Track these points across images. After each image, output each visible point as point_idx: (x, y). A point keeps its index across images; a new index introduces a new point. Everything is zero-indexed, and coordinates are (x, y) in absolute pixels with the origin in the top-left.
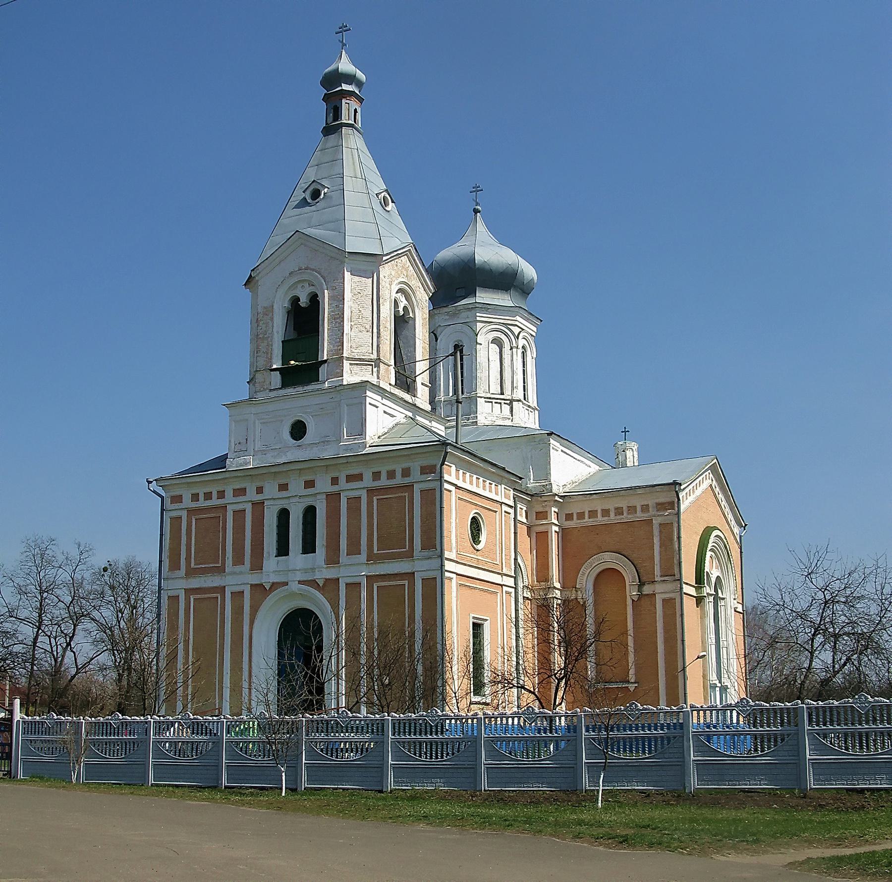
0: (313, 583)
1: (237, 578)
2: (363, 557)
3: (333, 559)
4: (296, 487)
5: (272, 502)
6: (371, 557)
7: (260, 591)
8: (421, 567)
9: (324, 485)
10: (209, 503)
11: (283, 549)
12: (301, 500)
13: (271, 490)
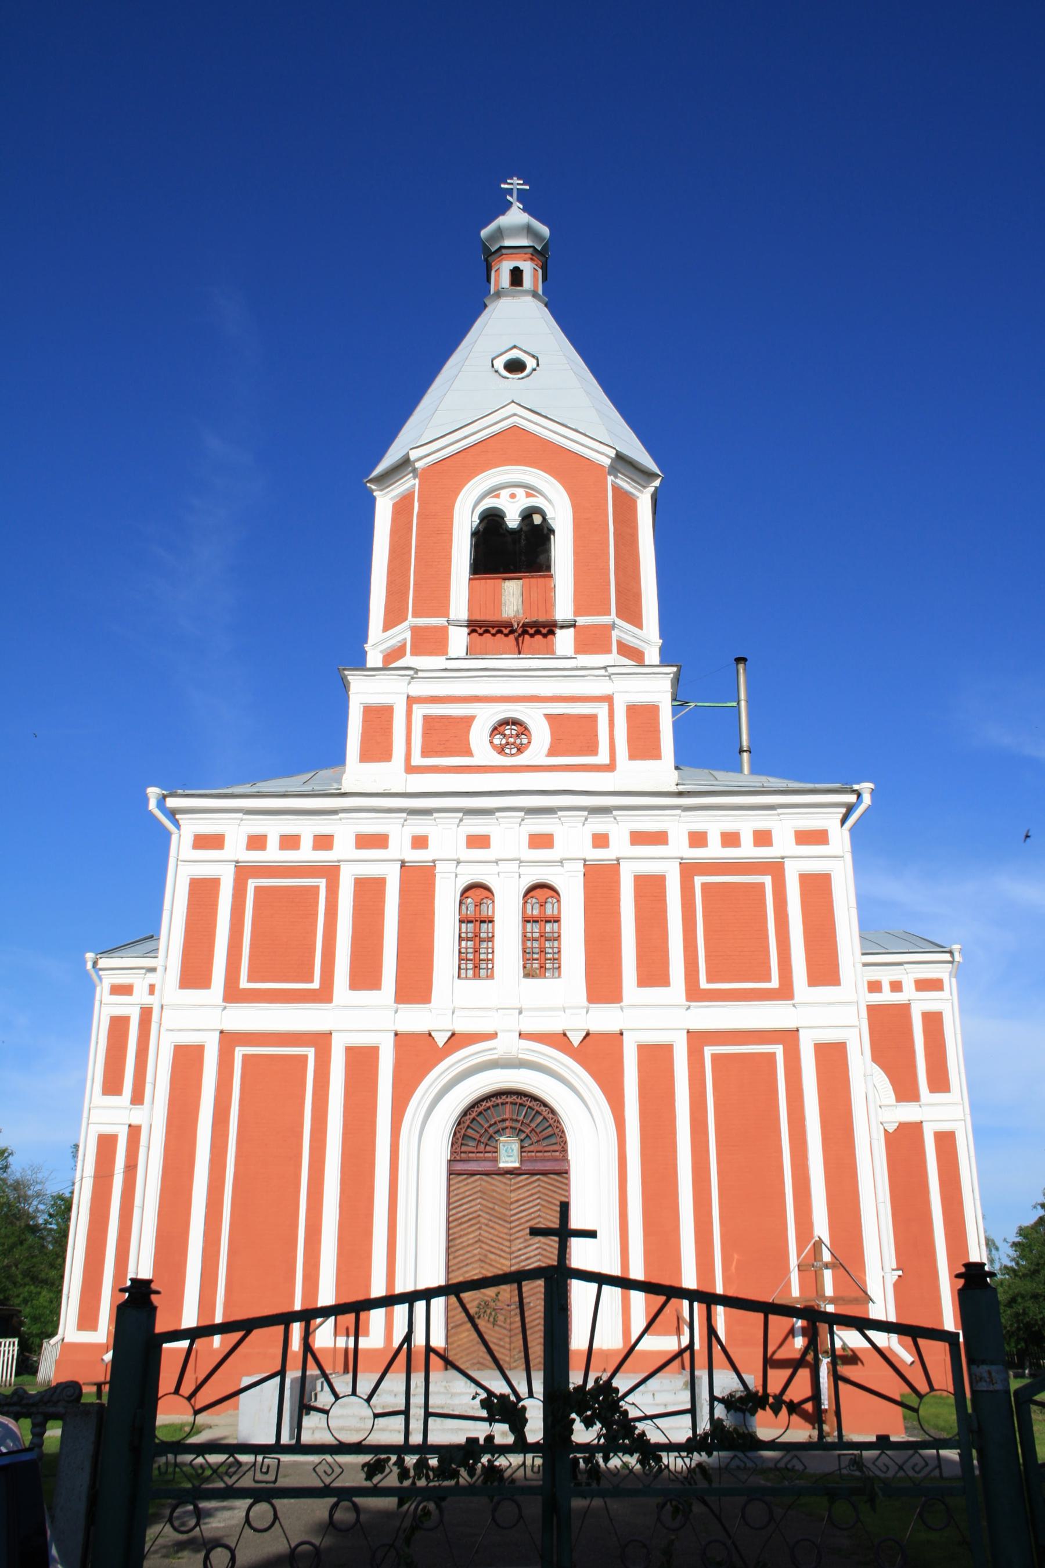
0: (559, 1040)
1: (363, 1018)
3: (603, 986)
4: (509, 835)
6: (694, 993)
7: (417, 1054)
10: (290, 856)
11: (476, 961)
12: (523, 870)
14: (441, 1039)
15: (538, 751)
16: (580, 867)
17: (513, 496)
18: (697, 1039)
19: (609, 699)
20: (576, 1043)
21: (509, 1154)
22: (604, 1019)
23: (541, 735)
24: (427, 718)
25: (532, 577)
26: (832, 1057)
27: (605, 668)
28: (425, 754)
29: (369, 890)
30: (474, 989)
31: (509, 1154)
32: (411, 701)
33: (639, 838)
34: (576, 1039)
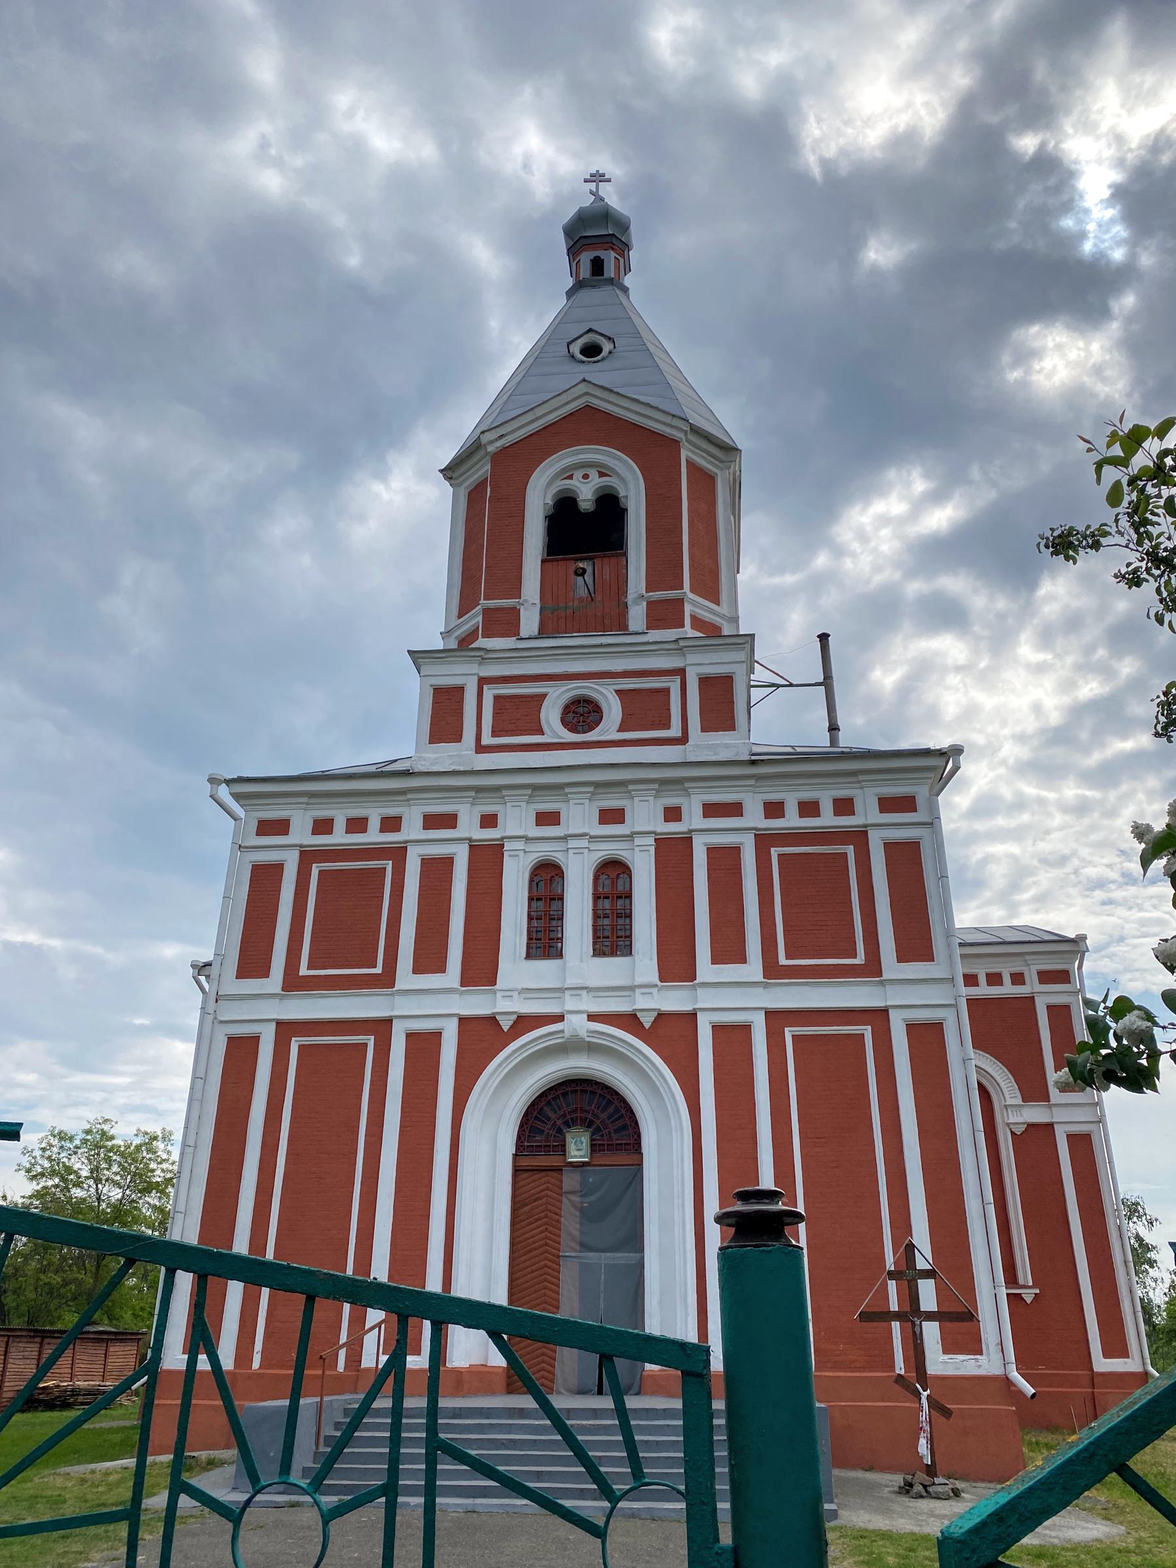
0: (629, 1021)
1: (429, 1001)
2: (753, 969)
3: (676, 964)
4: (579, 816)
5: (520, 845)
6: (772, 970)
7: (483, 1038)
8: (266, 1006)
9: (646, 816)
11: (545, 941)
13: (516, 820)
14: (506, 1024)
15: (610, 726)
16: (651, 840)
17: (586, 476)
18: (777, 1019)
19: (681, 672)
20: (647, 1025)
21: (578, 1148)
22: (674, 1000)
23: (613, 711)
24: (497, 698)
25: (605, 556)
26: (928, 1037)
27: (676, 641)
28: (495, 734)
29: (437, 872)
30: (544, 971)
31: (578, 1148)
32: (483, 681)
33: (710, 810)
34: (647, 1021)
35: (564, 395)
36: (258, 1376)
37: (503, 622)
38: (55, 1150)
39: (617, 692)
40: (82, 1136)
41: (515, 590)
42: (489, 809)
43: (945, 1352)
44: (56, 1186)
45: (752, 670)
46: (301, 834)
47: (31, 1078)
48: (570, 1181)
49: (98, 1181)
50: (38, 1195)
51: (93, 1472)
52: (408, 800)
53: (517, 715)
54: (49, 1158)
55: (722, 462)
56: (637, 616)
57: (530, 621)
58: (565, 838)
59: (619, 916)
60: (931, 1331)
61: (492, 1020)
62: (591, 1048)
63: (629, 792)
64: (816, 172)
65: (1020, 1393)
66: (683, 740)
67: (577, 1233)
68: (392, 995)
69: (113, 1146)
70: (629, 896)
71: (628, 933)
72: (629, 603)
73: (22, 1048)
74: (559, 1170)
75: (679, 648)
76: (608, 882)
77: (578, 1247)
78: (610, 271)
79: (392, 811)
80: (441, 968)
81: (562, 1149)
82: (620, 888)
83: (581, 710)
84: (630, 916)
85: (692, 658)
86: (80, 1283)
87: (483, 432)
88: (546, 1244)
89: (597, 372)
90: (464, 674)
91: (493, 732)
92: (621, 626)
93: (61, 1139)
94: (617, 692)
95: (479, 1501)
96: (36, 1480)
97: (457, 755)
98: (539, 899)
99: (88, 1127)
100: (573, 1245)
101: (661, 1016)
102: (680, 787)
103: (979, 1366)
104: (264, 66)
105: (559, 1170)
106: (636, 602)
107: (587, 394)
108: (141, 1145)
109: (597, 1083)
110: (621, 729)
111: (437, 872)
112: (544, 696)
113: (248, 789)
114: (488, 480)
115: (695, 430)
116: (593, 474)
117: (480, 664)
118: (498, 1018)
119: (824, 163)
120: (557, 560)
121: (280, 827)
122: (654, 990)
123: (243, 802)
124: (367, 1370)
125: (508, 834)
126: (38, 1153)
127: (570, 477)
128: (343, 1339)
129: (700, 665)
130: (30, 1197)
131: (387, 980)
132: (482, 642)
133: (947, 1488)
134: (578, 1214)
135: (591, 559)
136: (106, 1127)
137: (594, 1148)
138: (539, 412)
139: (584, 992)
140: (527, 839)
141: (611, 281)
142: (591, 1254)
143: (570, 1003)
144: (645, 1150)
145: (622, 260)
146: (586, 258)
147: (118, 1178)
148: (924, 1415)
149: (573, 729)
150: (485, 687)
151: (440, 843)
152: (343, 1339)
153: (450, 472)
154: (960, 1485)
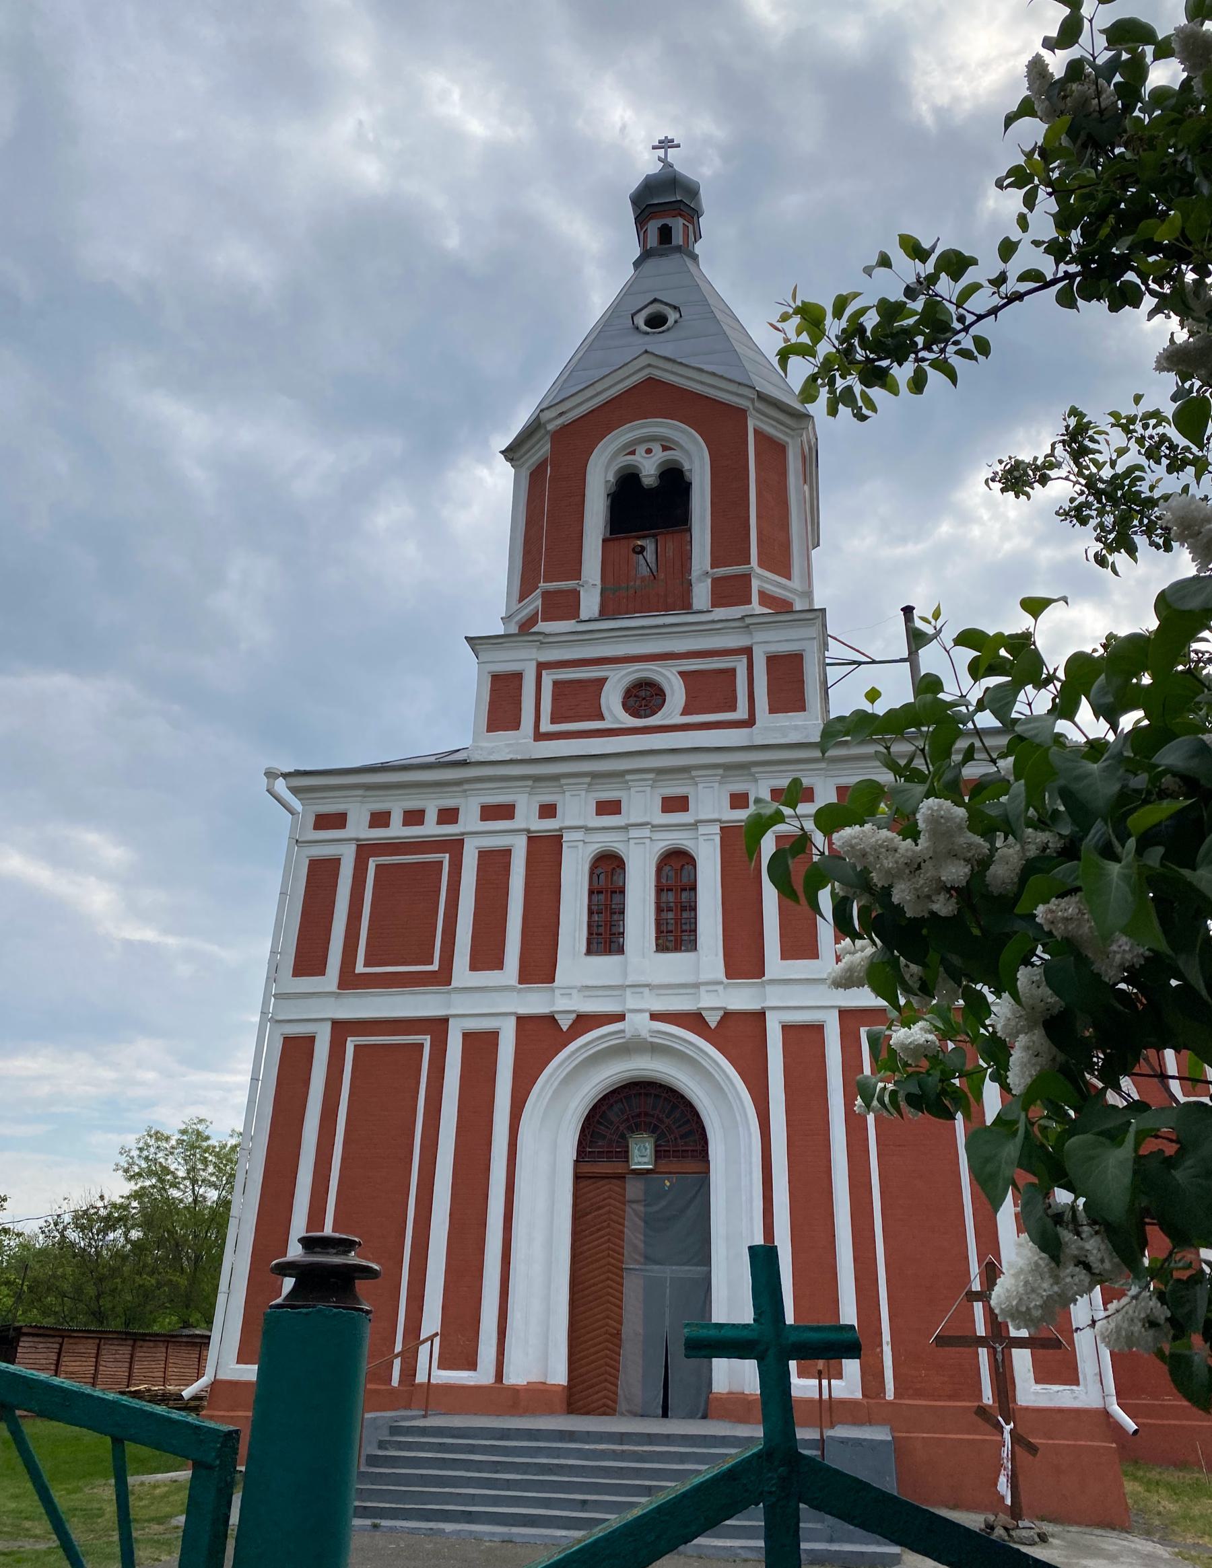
0: (693, 1021)
1: (486, 999)
3: (744, 960)
4: (642, 804)
5: (579, 835)
7: (541, 1037)
8: (324, 1004)
11: (606, 936)
12: (656, 836)
13: (576, 809)
14: (565, 1023)
17: (649, 451)
18: (341, 1029)
19: (748, 651)
21: (642, 1154)
22: (741, 998)
23: (676, 694)
24: (556, 684)
27: (743, 618)
29: (494, 864)
31: (642, 1154)
32: (541, 666)
34: (713, 1020)
35: (625, 368)
36: (890, 1403)
37: (563, 605)
38: (152, 1150)
39: (680, 673)
40: (177, 1136)
41: (576, 574)
42: (548, 799)
43: (1037, 1382)
44: (154, 1186)
45: (825, 647)
46: (358, 828)
47: (150, 1076)
48: (634, 1189)
49: (194, 1182)
50: (137, 1195)
51: (142, 1484)
52: (465, 791)
53: (577, 701)
54: (147, 1159)
55: (793, 430)
56: (701, 594)
57: (590, 603)
58: (626, 828)
59: (683, 909)
60: (1022, 1359)
61: (550, 1019)
62: (655, 1049)
63: (626, 782)
64: (929, 120)
65: (1118, 1427)
66: (750, 722)
67: (641, 1245)
68: (448, 993)
69: (208, 1147)
70: (694, 888)
71: (693, 927)
72: (693, 581)
73: (144, 1046)
74: (621, 1177)
75: (745, 625)
76: (672, 874)
77: (642, 1260)
78: (678, 238)
79: (449, 803)
80: (499, 965)
81: (625, 1155)
82: (685, 880)
83: (643, 694)
84: (695, 909)
85: (759, 636)
86: (174, 1286)
87: (542, 411)
88: (609, 1255)
89: (662, 344)
90: (523, 660)
91: (552, 719)
92: (684, 603)
93: (157, 1139)
94: (680, 673)
95: (515, 1530)
96: (86, 1490)
97: (515, 743)
98: (599, 892)
99: (183, 1127)
100: (637, 1257)
101: (728, 1016)
102: (686, 776)
103: (1075, 1398)
104: (355, 52)
105: (621, 1177)
106: (700, 580)
107: (649, 365)
108: (236, 1146)
109: (661, 1086)
110: (685, 712)
111: (494, 864)
112: (605, 680)
113: (304, 782)
114: (550, 460)
115: (762, 397)
116: (657, 448)
117: (539, 648)
118: (557, 1017)
119: (938, 111)
120: (617, 539)
121: (337, 821)
122: (720, 988)
123: (302, 796)
124: (421, 1385)
125: (567, 823)
126: (135, 1153)
127: (633, 453)
128: (398, 1348)
129: (772, 641)
130: (128, 1198)
131: (443, 977)
132: (542, 626)
133: (1032, 1533)
134: (642, 1224)
135: (654, 536)
136: (201, 1127)
137: (659, 1154)
138: (599, 387)
139: (646, 990)
140: (587, 829)
141: (679, 249)
142: (656, 1267)
143: (631, 1002)
144: (711, 1158)
145: (691, 227)
146: (653, 227)
147: (214, 1179)
148: (1006, 1452)
149: (635, 713)
150: (544, 672)
151: (496, 836)
152: (398, 1348)
153: (510, 453)
154: (1047, 1528)
